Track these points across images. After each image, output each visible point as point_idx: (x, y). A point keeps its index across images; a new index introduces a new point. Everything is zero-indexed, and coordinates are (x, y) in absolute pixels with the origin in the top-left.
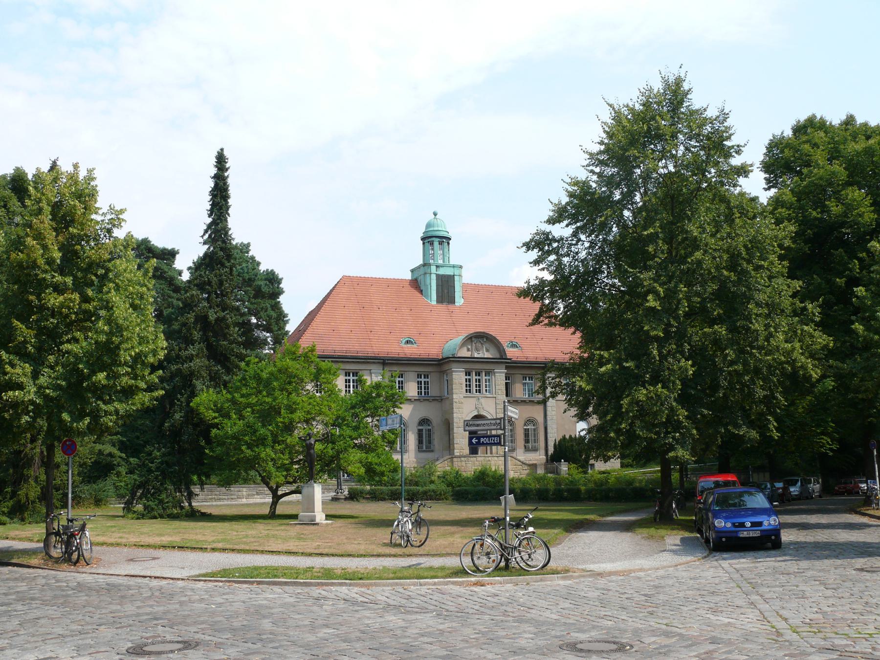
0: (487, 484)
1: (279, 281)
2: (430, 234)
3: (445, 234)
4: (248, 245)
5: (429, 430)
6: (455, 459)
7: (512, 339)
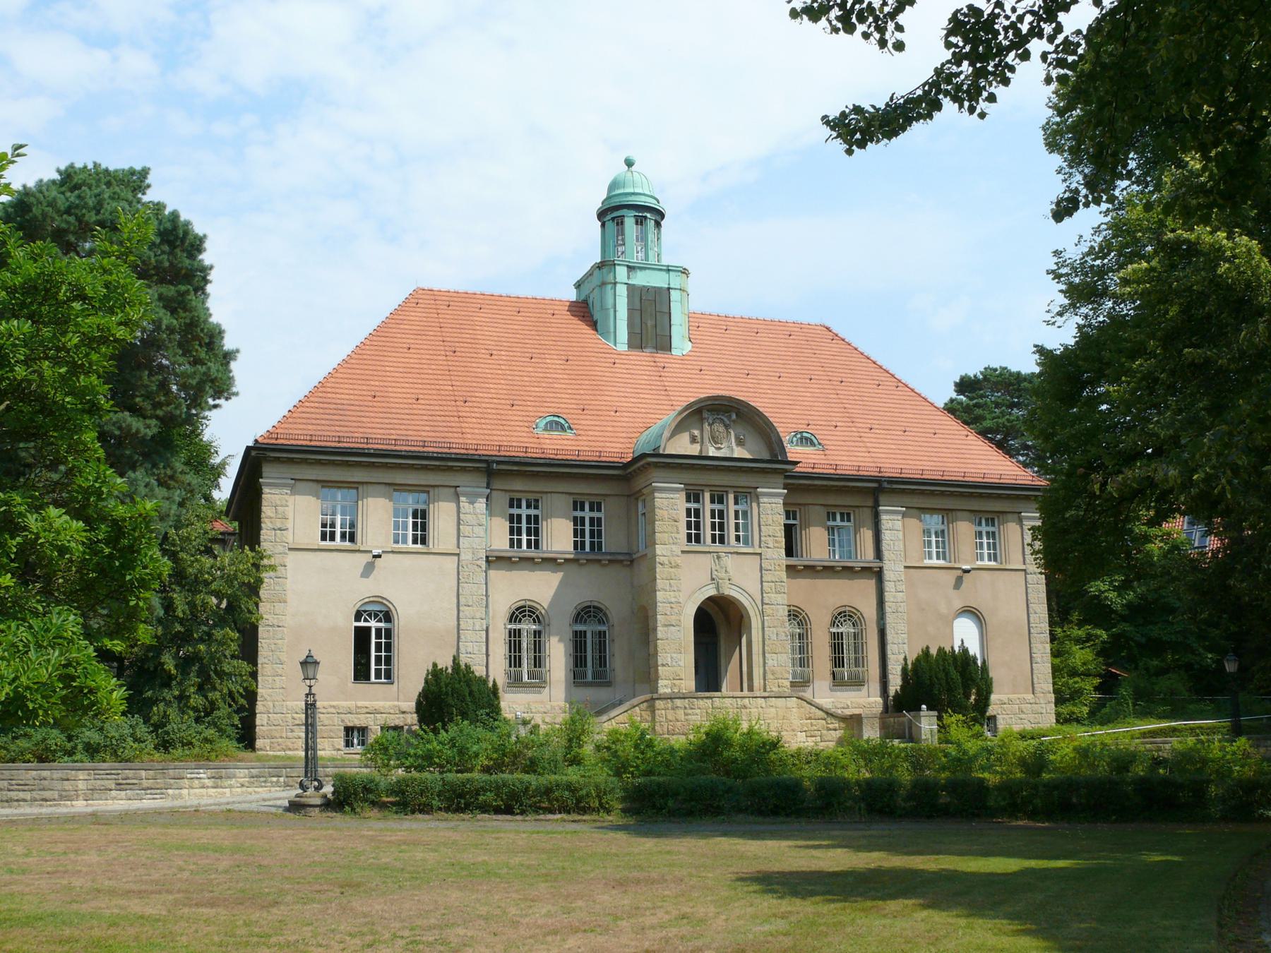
0: (729, 768)
1: (196, 245)
2: (616, 202)
3: (651, 203)
4: (144, 173)
5: (602, 634)
6: (659, 704)
7: (802, 428)
